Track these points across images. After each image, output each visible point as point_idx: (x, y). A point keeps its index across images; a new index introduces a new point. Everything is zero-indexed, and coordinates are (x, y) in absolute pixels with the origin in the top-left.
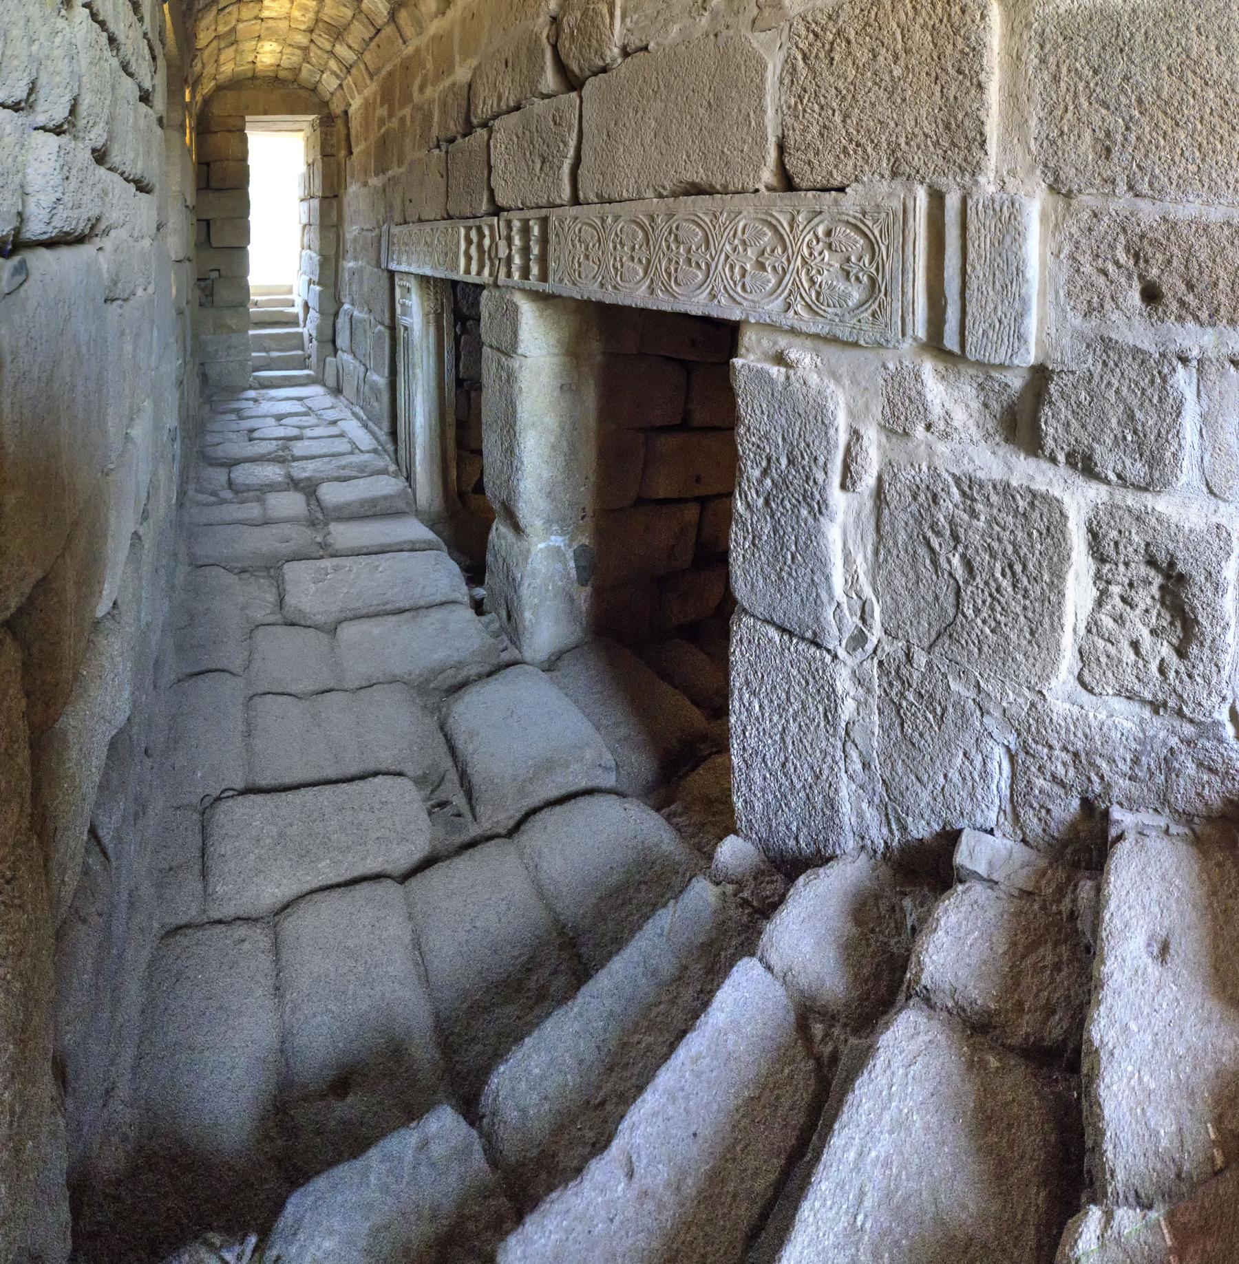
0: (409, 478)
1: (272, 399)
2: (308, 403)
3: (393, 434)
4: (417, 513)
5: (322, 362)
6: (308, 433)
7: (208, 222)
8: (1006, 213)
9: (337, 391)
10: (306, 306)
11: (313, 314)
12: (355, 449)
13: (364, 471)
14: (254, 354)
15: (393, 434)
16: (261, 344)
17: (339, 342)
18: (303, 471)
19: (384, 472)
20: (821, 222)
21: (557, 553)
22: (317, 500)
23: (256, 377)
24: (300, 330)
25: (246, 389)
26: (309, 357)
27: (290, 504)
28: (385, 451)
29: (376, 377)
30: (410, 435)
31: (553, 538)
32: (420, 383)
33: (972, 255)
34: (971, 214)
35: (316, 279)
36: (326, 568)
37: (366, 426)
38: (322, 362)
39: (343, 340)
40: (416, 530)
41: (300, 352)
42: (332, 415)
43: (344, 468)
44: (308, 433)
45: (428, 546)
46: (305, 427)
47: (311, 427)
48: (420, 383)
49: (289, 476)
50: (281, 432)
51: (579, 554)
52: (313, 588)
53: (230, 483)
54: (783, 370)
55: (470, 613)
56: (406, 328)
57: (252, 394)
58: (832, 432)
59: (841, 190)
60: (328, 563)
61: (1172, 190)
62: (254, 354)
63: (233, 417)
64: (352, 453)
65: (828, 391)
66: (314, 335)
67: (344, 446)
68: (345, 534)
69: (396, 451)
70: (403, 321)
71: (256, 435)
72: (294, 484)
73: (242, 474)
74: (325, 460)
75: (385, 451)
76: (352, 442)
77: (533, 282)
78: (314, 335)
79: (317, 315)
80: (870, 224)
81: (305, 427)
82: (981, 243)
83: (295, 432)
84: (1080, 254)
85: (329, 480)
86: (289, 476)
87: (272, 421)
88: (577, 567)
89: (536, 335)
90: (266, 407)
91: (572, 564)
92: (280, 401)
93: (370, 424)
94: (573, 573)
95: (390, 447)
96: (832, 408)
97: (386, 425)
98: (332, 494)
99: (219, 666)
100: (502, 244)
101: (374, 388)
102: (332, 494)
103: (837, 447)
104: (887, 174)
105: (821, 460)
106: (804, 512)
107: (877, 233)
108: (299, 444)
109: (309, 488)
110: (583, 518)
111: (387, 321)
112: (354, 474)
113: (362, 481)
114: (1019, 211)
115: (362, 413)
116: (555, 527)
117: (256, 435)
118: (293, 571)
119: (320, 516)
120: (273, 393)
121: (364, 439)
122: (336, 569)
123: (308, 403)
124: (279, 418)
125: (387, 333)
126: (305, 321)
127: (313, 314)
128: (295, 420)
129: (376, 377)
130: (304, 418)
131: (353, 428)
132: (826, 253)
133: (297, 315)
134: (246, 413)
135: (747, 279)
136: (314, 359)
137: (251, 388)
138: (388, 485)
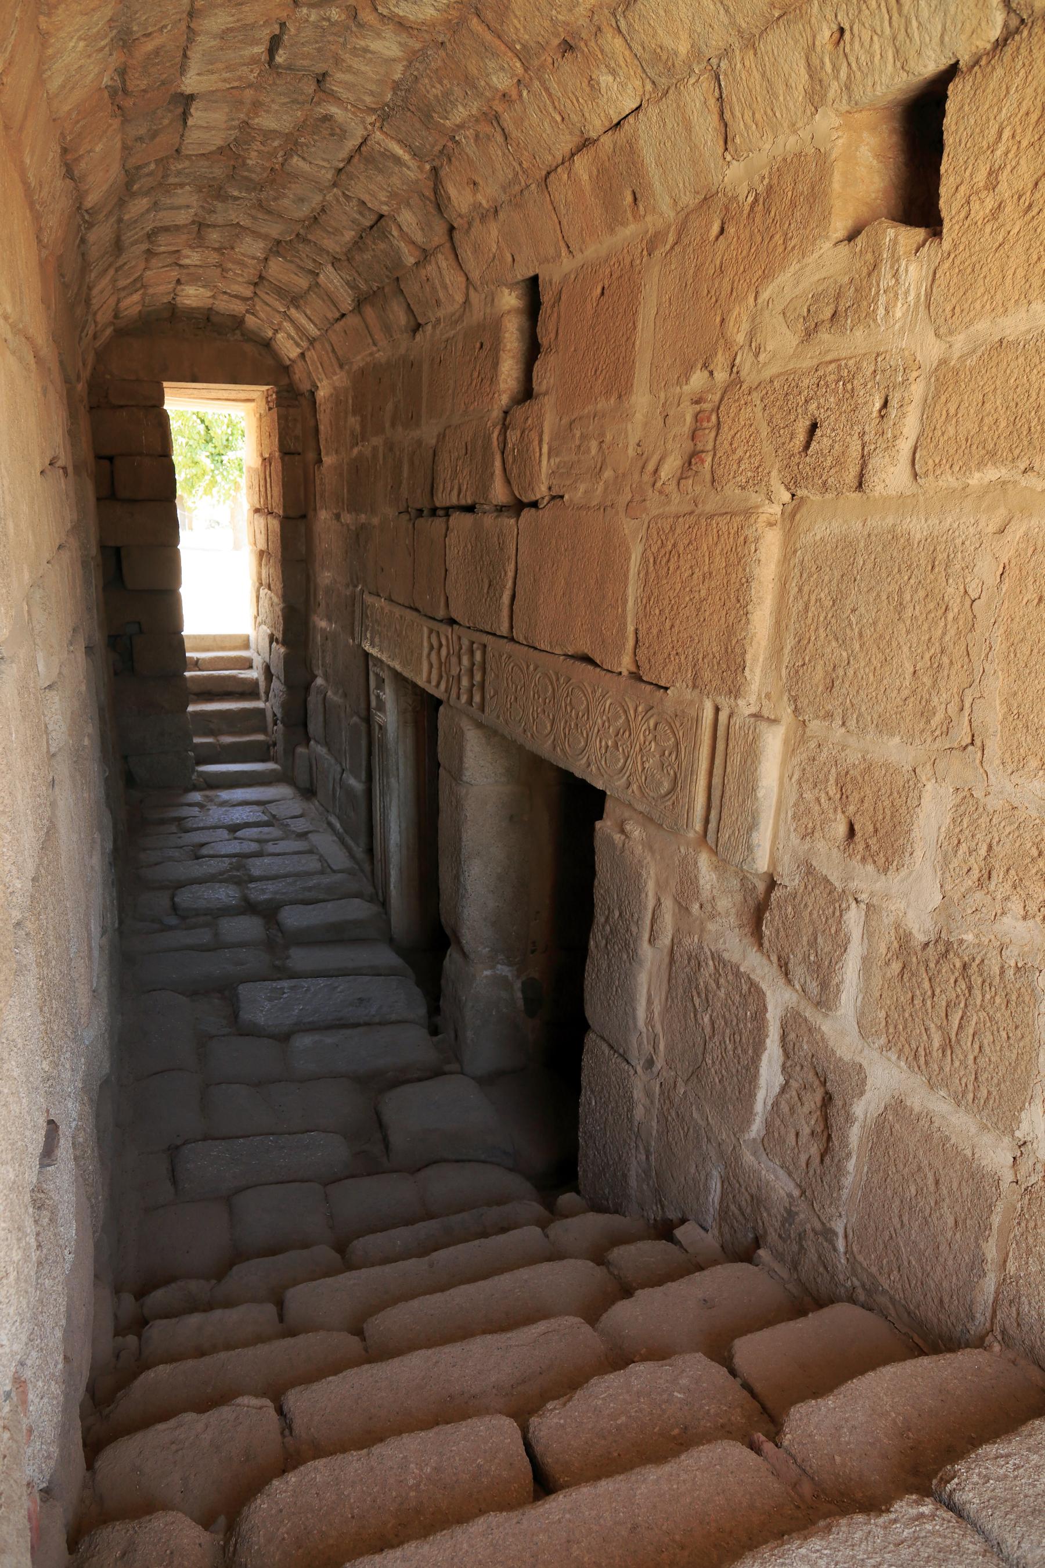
0: (384, 904)
1: (223, 804)
2: (273, 809)
3: (370, 851)
4: (391, 941)
5: (290, 752)
6: (270, 848)
7: (118, 551)
8: (751, 737)
9: (308, 792)
10: (267, 669)
11: (276, 684)
12: (326, 868)
13: (334, 894)
14: (197, 740)
15: (370, 851)
16: (209, 723)
17: (311, 728)
18: (262, 893)
19: (358, 895)
20: (652, 716)
21: (504, 983)
22: (278, 924)
23: (201, 774)
24: (260, 704)
25: (187, 790)
26: (275, 744)
27: (247, 927)
28: (362, 871)
29: (352, 781)
30: (385, 851)
31: (499, 966)
32: (395, 795)
33: (729, 769)
34: (732, 735)
35: (279, 635)
36: (282, 988)
37: (343, 842)
38: (290, 752)
39: (315, 726)
40: (386, 957)
41: (261, 737)
42: (300, 825)
43: (310, 889)
44: (270, 848)
45: (392, 972)
46: (267, 841)
47: (275, 840)
48: (395, 795)
49: (245, 899)
50: (234, 847)
51: (528, 986)
52: (267, 1005)
53: (175, 907)
54: (623, 837)
55: (424, 1032)
56: (380, 727)
57: (197, 796)
58: (643, 895)
59: (666, 689)
60: (286, 984)
61: (871, 729)
62: (197, 740)
63: (174, 828)
64: (322, 872)
65: (645, 862)
66: (279, 715)
67: (313, 864)
68: (300, 958)
69: (373, 871)
70: (379, 718)
71: (204, 851)
72: (249, 907)
73: (185, 898)
74: (289, 880)
75: (362, 871)
76: (322, 859)
77: (474, 709)
78: (279, 715)
79: (282, 687)
80: (678, 725)
81: (267, 841)
82: (735, 759)
83: (254, 847)
84: (808, 769)
85: (292, 903)
86: (245, 899)
87: (225, 834)
88: (525, 999)
89: (482, 763)
90: (216, 815)
91: (519, 995)
92: (236, 806)
93: (348, 839)
94: (520, 1003)
95: (367, 867)
96: (645, 876)
97: (363, 840)
98: (293, 918)
99: (522, 1449)
100: (454, 660)
101: (349, 792)
102: (293, 918)
103: (646, 909)
104: (690, 684)
105: (636, 916)
106: (625, 956)
107: (681, 734)
108: (257, 861)
109: (269, 912)
110: (533, 952)
111: (363, 713)
112: (321, 896)
113: (330, 905)
114: (759, 735)
115: (338, 826)
116: (501, 957)
117: (204, 851)
118: (244, 990)
119: (278, 940)
120: (225, 795)
121: (339, 858)
122: (292, 988)
123: (273, 809)
124: (234, 828)
125: (363, 727)
126: (267, 693)
127: (276, 684)
128: (253, 832)
129: (352, 781)
130: (266, 829)
131: (326, 843)
132: (653, 744)
133: (255, 683)
134: (190, 824)
135: (608, 754)
136: (280, 748)
137: (195, 788)
138: (358, 910)
